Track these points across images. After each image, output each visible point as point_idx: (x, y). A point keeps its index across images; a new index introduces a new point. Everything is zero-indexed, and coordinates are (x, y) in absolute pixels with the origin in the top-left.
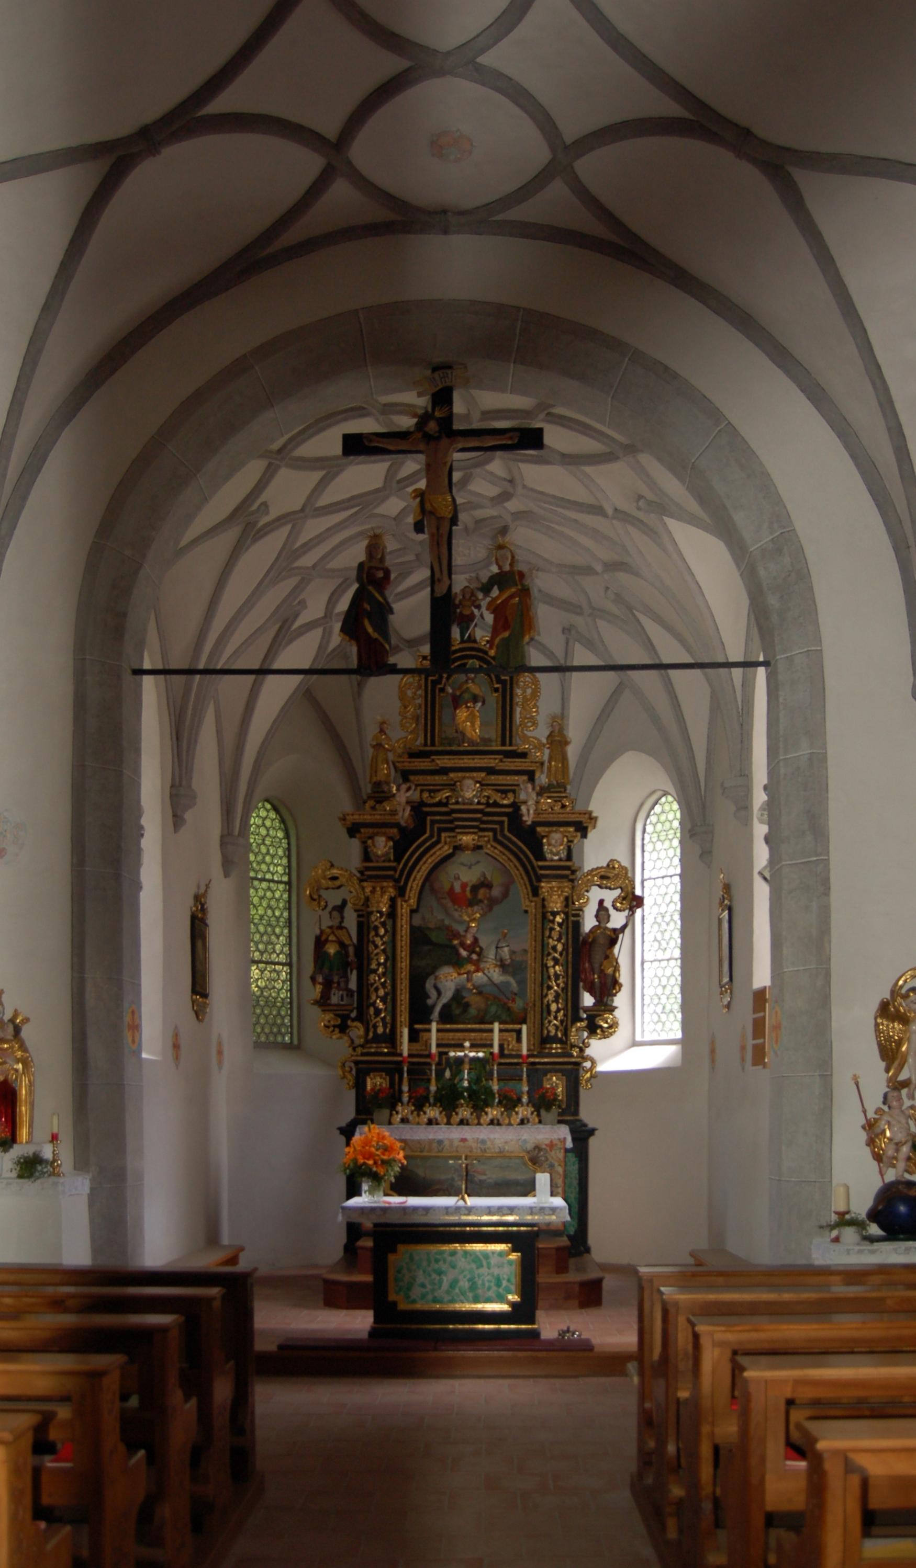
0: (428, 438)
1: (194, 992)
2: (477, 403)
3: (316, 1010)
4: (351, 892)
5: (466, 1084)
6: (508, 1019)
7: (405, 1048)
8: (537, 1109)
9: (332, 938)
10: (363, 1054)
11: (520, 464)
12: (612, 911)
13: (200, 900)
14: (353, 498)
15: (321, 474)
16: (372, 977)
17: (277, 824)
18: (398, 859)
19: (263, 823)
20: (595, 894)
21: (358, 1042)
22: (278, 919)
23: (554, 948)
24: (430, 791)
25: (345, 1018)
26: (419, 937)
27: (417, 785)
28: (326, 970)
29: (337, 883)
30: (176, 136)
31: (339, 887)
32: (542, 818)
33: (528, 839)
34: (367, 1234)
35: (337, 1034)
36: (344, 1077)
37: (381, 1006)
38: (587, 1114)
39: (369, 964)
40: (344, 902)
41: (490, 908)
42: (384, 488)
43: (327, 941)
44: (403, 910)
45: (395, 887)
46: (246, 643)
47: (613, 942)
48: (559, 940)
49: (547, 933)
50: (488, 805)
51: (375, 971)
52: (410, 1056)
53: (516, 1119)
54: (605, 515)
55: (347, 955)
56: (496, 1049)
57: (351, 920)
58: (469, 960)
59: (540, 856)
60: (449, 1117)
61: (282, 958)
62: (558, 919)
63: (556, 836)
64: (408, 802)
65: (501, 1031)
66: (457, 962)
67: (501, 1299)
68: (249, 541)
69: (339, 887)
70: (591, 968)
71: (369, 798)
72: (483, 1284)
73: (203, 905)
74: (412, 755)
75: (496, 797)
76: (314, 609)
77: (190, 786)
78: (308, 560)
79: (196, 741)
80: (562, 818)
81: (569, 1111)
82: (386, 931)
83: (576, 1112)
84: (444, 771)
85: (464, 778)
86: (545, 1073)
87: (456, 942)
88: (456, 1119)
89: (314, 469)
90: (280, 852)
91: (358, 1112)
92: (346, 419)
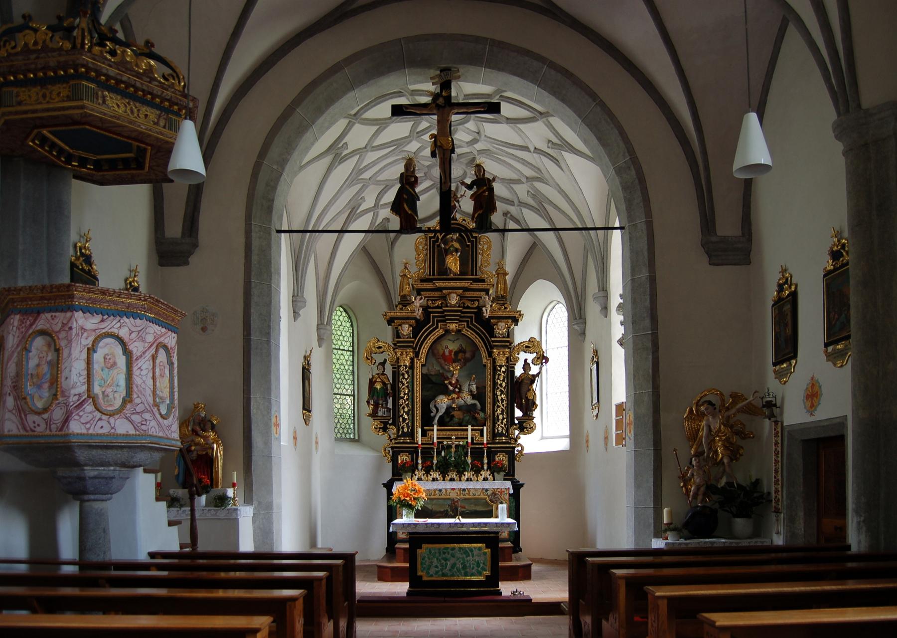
0: (438, 107)
1: (304, 409)
2: (467, 88)
4: (388, 355)
7: (419, 439)
8: (493, 474)
9: (378, 380)
12: (532, 365)
14: (392, 141)
16: (401, 401)
17: (346, 319)
18: (415, 337)
19: (340, 318)
20: (522, 356)
21: (392, 437)
23: (501, 385)
25: (386, 424)
26: (426, 378)
29: (382, 350)
32: (495, 314)
33: (487, 326)
34: (403, 541)
37: (406, 417)
38: (519, 476)
39: (399, 394)
40: (385, 360)
42: (409, 136)
43: (376, 381)
44: (418, 364)
46: (333, 219)
47: (533, 381)
48: (503, 381)
50: (464, 308)
51: (403, 398)
53: (481, 478)
55: (387, 389)
56: (470, 440)
57: (389, 371)
58: (454, 392)
59: (492, 335)
61: (349, 392)
62: (503, 369)
63: (502, 324)
66: (446, 392)
67: (480, 574)
70: (521, 393)
71: (399, 304)
74: (423, 281)
75: (469, 304)
76: (369, 202)
78: (367, 175)
80: (505, 314)
81: (509, 474)
83: (513, 475)
84: (440, 289)
86: (496, 453)
88: (448, 478)
90: (348, 334)
91: (393, 475)
92: (391, 98)
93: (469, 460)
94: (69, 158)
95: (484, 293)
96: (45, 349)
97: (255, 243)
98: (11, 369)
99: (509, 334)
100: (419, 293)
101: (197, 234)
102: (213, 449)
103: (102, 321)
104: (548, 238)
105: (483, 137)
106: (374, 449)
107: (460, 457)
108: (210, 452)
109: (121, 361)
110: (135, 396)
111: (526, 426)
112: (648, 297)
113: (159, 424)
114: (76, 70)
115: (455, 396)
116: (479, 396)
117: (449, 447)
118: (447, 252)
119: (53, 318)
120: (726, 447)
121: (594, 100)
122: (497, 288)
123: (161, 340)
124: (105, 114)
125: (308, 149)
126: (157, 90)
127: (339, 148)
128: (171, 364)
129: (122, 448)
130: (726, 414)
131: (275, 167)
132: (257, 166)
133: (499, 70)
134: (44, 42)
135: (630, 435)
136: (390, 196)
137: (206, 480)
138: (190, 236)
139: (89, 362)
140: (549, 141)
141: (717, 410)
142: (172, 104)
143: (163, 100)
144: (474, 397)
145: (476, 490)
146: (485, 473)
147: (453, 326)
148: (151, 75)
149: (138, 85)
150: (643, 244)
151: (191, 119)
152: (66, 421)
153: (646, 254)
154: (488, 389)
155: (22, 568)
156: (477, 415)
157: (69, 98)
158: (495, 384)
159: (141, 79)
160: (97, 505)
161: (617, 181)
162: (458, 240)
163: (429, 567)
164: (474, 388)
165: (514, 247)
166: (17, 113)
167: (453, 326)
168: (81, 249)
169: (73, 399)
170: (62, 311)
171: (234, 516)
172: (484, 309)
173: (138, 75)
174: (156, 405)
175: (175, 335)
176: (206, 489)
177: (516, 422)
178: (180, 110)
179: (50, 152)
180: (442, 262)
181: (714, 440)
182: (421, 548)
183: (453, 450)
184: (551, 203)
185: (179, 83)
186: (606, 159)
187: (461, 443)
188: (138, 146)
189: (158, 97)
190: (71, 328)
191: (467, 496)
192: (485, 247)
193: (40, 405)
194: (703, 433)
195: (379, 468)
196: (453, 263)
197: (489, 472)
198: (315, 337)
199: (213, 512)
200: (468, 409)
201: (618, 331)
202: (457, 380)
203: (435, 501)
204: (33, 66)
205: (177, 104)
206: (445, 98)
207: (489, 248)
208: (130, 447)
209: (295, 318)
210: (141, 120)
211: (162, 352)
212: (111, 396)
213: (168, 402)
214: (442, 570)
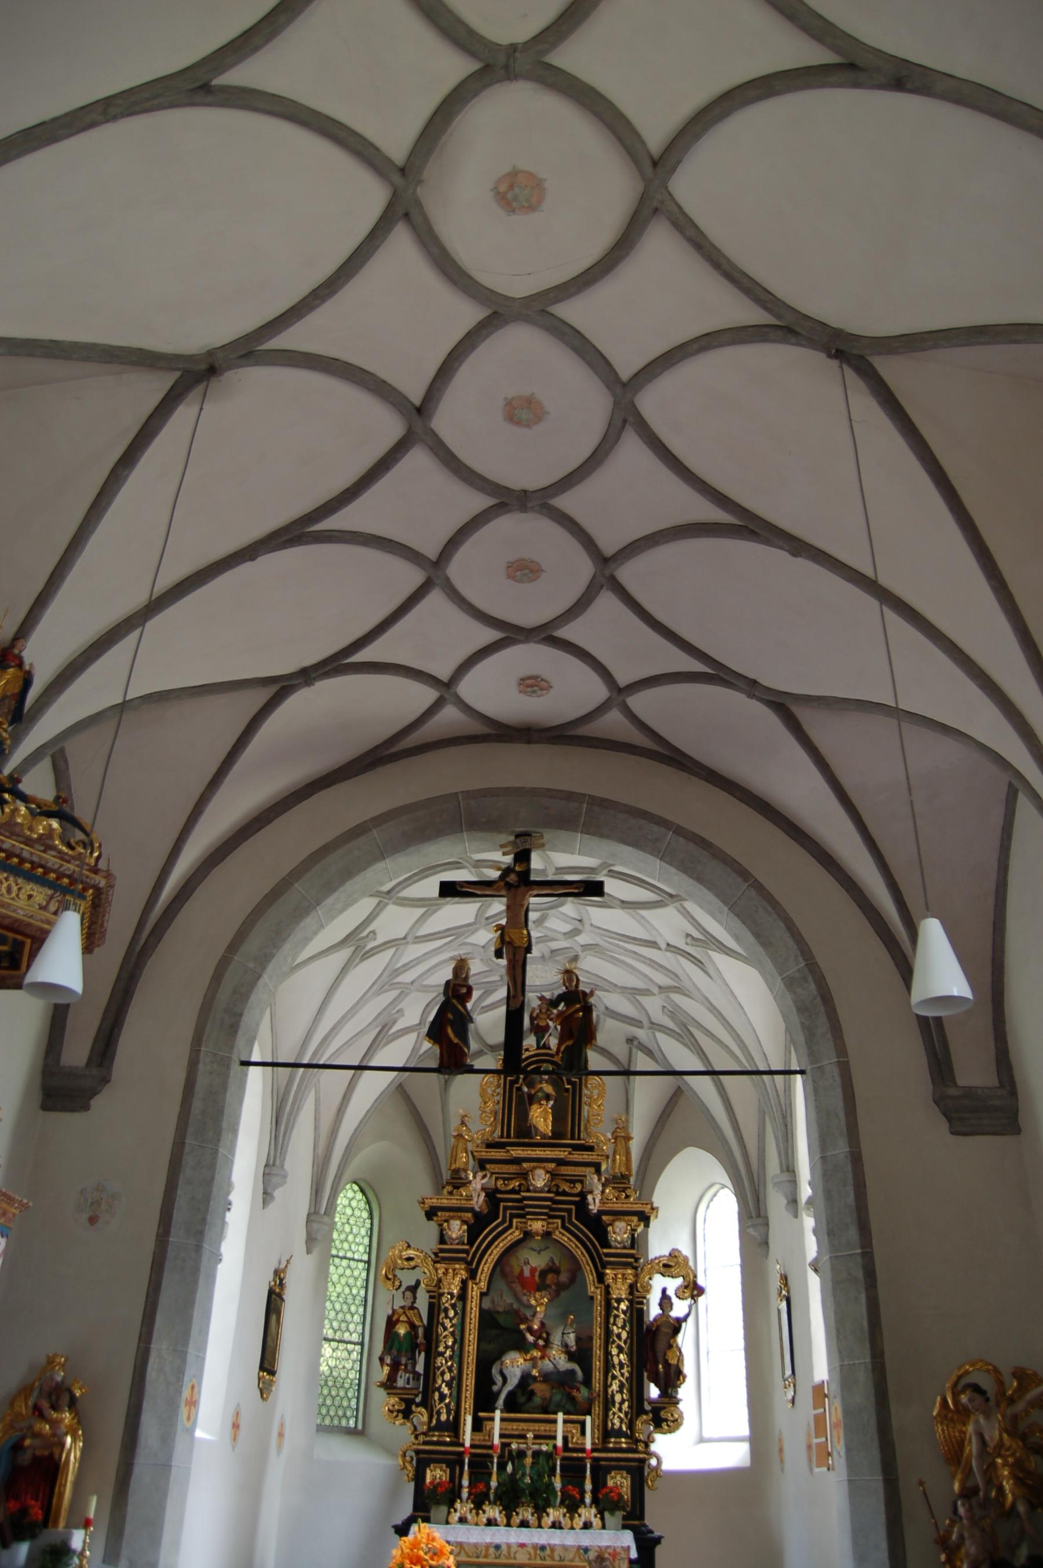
0: (509, 886)
1: (262, 1368)
3: (382, 1393)
5: (528, 1480)
7: (467, 1436)
8: (601, 1513)
9: (403, 1318)
10: (425, 1443)
11: (588, 908)
12: (675, 1300)
13: (279, 1275)
15: (422, 910)
17: (362, 1205)
18: (471, 1243)
19: (350, 1202)
20: (659, 1283)
22: (354, 1297)
23: (619, 1336)
24: (504, 1179)
26: (487, 1319)
28: (394, 1352)
29: (413, 1263)
30: (327, 675)
31: (414, 1268)
32: (609, 1207)
33: (596, 1227)
35: (400, 1420)
36: (404, 1468)
37: (446, 1390)
38: (654, 1520)
39: (437, 1347)
40: (418, 1283)
41: (557, 1294)
43: (398, 1321)
44: (474, 1291)
46: (348, 1043)
48: (623, 1328)
49: (612, 1320)
50: (558, 1193)
51: (442, 1354)
52: (472, 1446)
53: (579, 1522)
54: (660, 949)
55: (416, 1336)
56: (559, 1442)
57: (422, 1302)
58: (535, 1346)
59: (605, 1244)
61: (355, 1337)
62: (623, 1306)
63: (620, 1225)
64: (483, 1189)
65: (565, 1422)
66: (522, 1346)
68: (357, 960)
69: (414, 1268)
70: (655, 1352)
73: (281, 1280)
75: (565, 1187)
77: (282, 1166)
78: (407, 977)
79: (293, 1126)
80: (626, 1207)
82: (456, 1313)
83: (641, 1517)
84: (517, 1161)
85: (535, 1168)
86: (608, 1470)
87: (522, 1327)
88: (516, 1520)
90: (363, 1231)
93: (558, 1483)
95: (592, 1169)
97: (202, 1081)
99: (637, 1243)
101: (112, 1063)
102: (63, 1445)
104: (703, 1086)
105: (587, 927)
106: (389, 1451)
107: (540, 1476)
108: (56, 1451)
111: (664, 1416)
112: (850, 1189)
115: (536, 1354)
116: (581, 1355)
117: (521, 1454)
118: (532, 1099)
120: (1018, 1481)
121: (746, 880)
122: (614, 1160)
125: (307, 940)
126: (51, 859)
127: (363, 938)
130: (1010, 1411)
131: (251, 965)
133: (602, 836)
135: (838, 1449)
138: (100, 1065)
140: (688, 935)
141: (992, 1403)
142: (73, 881)
143: (61, 876)
144: (571, 1356)
145: (565, 1548)
146: (587, 1513)
147: (537, 1226)
148: (49, 842)
149: (25, 854)
150: (836, 1100)
153: (842, 1115)
154: (597, 1343)
156: (575, 1393)
158: (608, 1333)
159: (31, 846)
161: (789, 1000)
165: (646, 1097)
167: (537, 1226)
172: (590, 1197)
173: (28, 842)
177: (647, 1407)
178: (85, 890)
180: (523, 1115)
181: (993, 1465)
183: (529, 1461)
184: (699, 1026)
185: (92, 853)
186: (770, 965)
187: (544, 1448)
188: (15, 940)
189: (54, 871)
192: (596, 1092)
194: (972, 1448)
195: (393, 1494)
196: (541, 1118)
197: (593, 1511)
200: (561, 1380)
201: (811, 1247)
202: (543, 1324)
206: (519, 874)
207: (601, 1095)
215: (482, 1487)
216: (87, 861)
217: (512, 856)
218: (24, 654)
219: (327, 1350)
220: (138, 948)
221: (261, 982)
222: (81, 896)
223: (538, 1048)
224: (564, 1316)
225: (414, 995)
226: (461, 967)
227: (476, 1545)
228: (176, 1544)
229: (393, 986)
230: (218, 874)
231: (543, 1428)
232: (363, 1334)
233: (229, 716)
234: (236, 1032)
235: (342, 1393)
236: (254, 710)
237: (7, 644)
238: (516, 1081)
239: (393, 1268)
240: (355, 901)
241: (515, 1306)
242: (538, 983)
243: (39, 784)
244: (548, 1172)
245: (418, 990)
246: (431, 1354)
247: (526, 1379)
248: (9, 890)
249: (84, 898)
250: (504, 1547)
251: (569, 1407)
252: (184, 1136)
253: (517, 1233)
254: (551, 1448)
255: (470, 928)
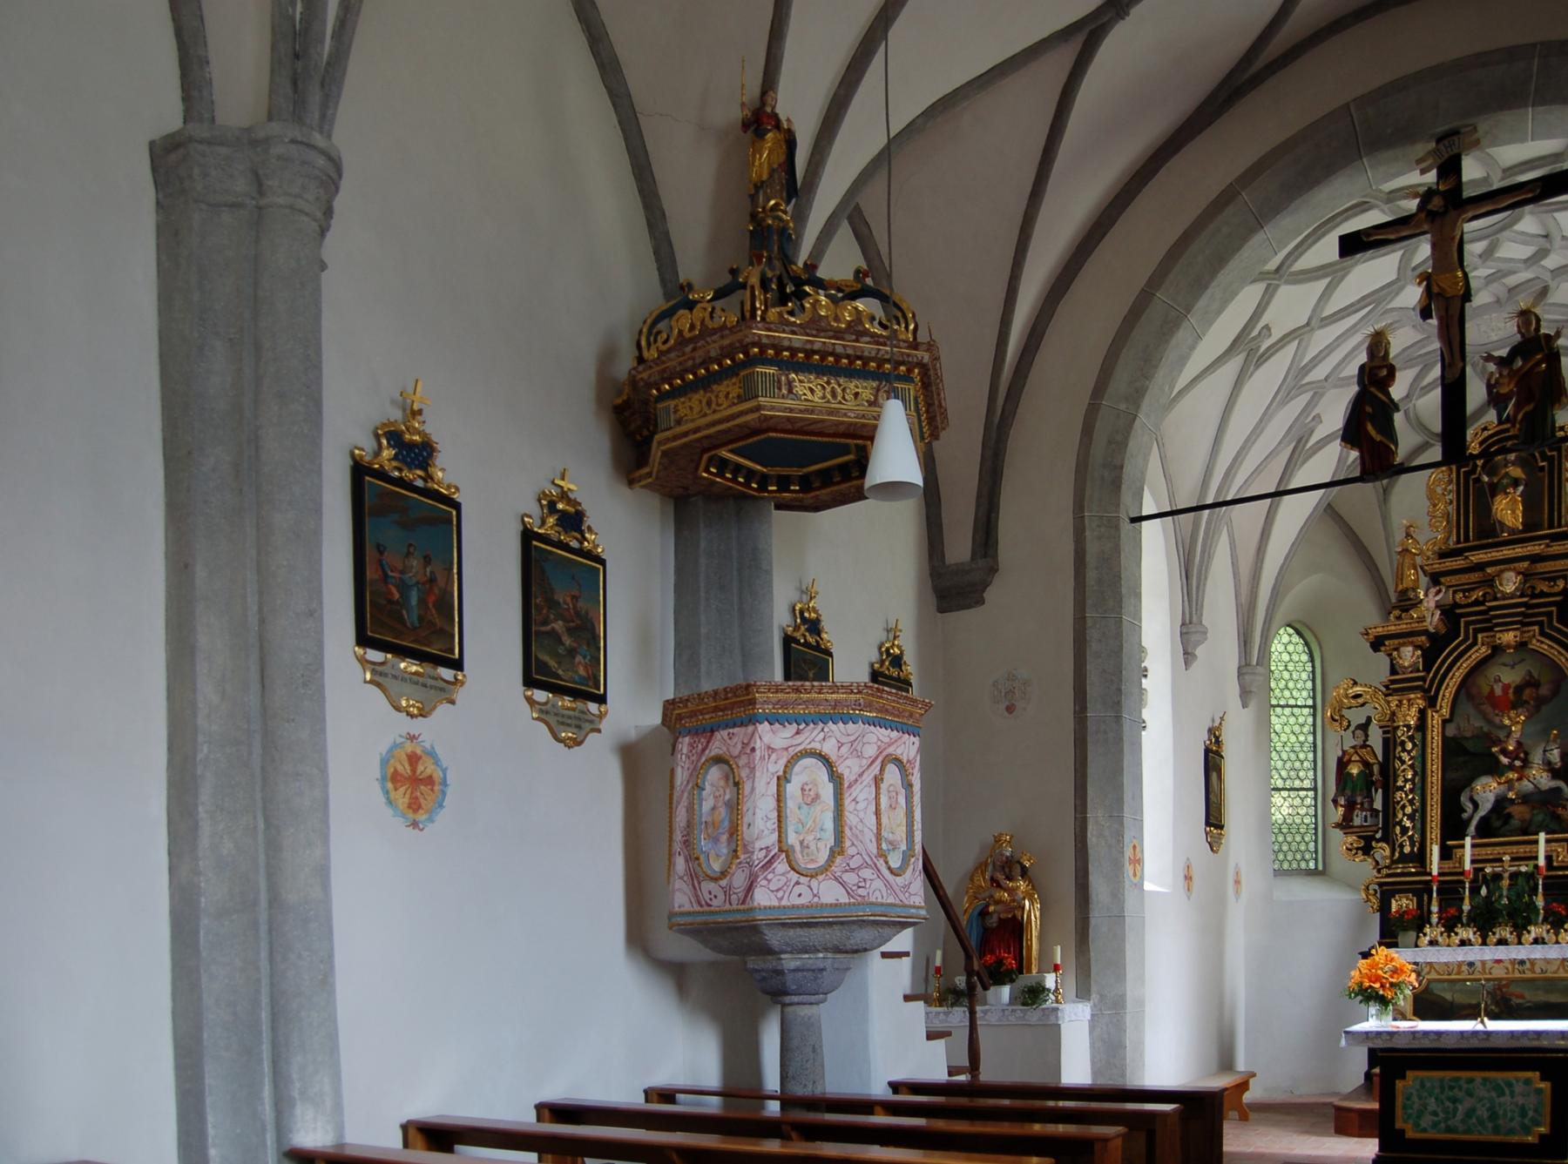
0: (1432, 216)
1: (1208, 824)
3: (1338, 833)
5: (1505, 901)
6: (1557, 828)
10: (1388, 876)
11: (1556, 215)
13: (1215, 735)
14: (1363, 298)
16: (1398, 795)
17: (1300, 648)
18: (1427, 668)
19: (1286, 649)
21: (1382, 863)
22: (1302, 744)
24: (1464, 591)
26: (1451, 747)
27: (1448, 587)
28: (1348, 792)
29: (1360, 701)
31: (1363, 705)
35: (1360, 857)
36: (1368, 900)
37: (1408, 824)
40: (1369, 719)
41: (1538, 708)
42: (1398, 279)
43: (1350, 761)
44: (1435, 720)
45: (1423, 698)
46: (1258, 470)
50: (1533, 596)
51: (1401, 788)
52: (1440, 874)
55: (1372, 774)
56: (1542, 862)
57: (1376, 738)
58: (1511, 767)
60: (1519, 937)
61: (1307, 784)
64: (1437, 607)
65: (1548, 841)
66: (1495, 769)
69: (1363, 705)
72: (1505, 1114)
73: (1217, 738)
78: (1319, 373)
82: (1414, 745)
84: (1480, 567)
85: (1502, 571)
87: (1495, 749)
89: (1318, 278)
90: (1304, 676)
93: (1540, 902)
94: (764, 481)
96: (722, 783)
97: (1092, 549)
98: (681, 816)
100: (1435, 579)
103: (798, 733)
105: (1557, 242)
106: (1352, 887)
107: (1519, 896)
108: (1018, 914)
109: (827, 791)
110: (848, 843)
113: (887, 884)
114: (746, 354)
115: (1513, 775)
117: (1497, 877)
118: (1494, 490)
119: (731, 736)
123: (890, 750)
124: (791, 410)
125: (1183, 360)
127: (1254, 338)
128: (908, 786)
129: (830, 924)
131: (1123, 407)
132: (1092, 411)
134: (703, 322)
136: (1334, 413)
137: (1011, 962)
139: (780, 798)
144: (1555, 773)
149: (839, 350)
151: (896, 397)
152: (750, 889)
155: (713, 1105)
157: (741, 399)
160: (804, 1011)
162: (1520, 462)
163: (1420, 1114)
164: (1555, 756)
166: (675, 438)
167: (1509, 637)
168: (802, 612)
169: (759, 856)
170: (742, 725)
171: (1052, 1020)
173: (838, 334)
174: (882, 854)
175: (916, 740)
176: (999, 976)
178: (909, 371)
179: (734, 480)
180: (1485, 510)
182: (1403, 1077)
183: (1505, 883)
185: (907, 328)
187: (1523, 869)
189: (872, 359)
190: (753, 750)
191: (1529, 975)
193: (717, 867)
195: (1360, 924)
196: (1508, 510)
198: (1236, 689)
199: (1019, 1014)
202: (1519, 744)
203: (1458, 986)
204: (690, 363)
205: (903, 363)
206: (1444, 194)
208: (842, 923)
209: (1187, 664)
210: (850, 404)
211: (892, 769)
212: (813, 847)
213: (904, 847)
214: (1446, 1120)
215: (1453, 911)
216: (902, 337)
217: (1434, 172)
218: (778, 110)
219: (1277, 799)
220: (996, 420)
221: (1137, 422)
222: (907, 378)
223: (1500, 422)
224: (1545, 732)
225: (1331, 394)
226: (1377, 344)
227: (1446, 964)
228: (1141, 978)
229: (1299, 389)
230: (1064, 309)
231: (1522, 850)
232: (1315, 780)
233: (1030, 100)
234: (1119, 488)
235: (1298, 838)
236: (1063, 77)
237: (758, 104)
238: (1473, 471)
239: (1339, 708)
240: (1235, 294)
241: (1485, 729)
242: (1495, 338)
243: (841, 263)
244: (1519, 573)
245: (1335, 387)
246: (1389, 786)
247: (1501, 803)
248: (834, 394)
249: (911, 380)
250: (1478, 965)
251: (1553, 826)
252: (1084, 610)
253: (1484, 649)
254: (1531, 869)
255: (1393, 288)
